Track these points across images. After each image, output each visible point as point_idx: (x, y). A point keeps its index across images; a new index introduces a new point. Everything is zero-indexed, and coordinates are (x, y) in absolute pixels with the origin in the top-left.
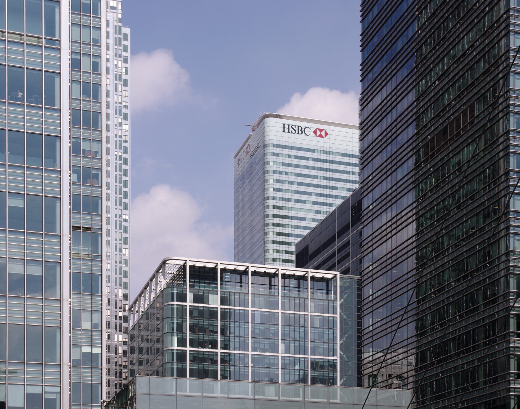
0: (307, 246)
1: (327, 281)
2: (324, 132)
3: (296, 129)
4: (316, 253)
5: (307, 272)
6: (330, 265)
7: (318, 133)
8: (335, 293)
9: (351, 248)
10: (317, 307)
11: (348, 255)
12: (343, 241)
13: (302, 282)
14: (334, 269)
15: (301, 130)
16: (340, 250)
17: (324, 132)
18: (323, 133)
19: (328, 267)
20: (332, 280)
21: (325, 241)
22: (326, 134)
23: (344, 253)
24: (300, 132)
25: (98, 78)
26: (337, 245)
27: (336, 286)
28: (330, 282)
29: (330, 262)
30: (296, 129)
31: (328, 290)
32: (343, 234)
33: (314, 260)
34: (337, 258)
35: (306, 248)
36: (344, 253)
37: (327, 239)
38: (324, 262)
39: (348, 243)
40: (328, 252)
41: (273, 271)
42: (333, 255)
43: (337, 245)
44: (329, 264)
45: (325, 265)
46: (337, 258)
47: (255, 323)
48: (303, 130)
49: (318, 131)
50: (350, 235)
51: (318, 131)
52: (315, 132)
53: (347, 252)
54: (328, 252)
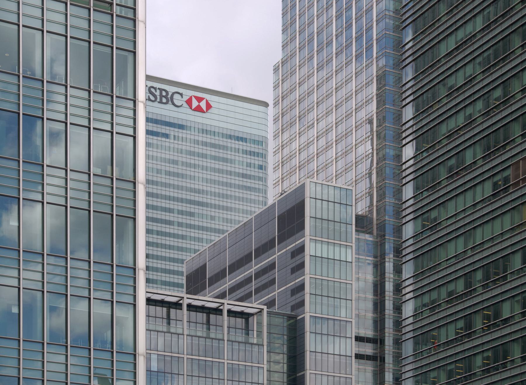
0: (205, 266)
1: (245, 316)
2: (204, 102)
3: (158, 93)
4: (220, 276)
5: (182, 298)
6: (242, 294)
7: (195, 103)
8: (260, 333)
9: (276, 274)
10: (195, 348)
11: (272, 282)
12: (265, 263)
13: (173, 311)
14: (249, 300)
15: (166, 97)
16: (258, 275)
17: (204, 102)
18: (203, 105)
19: (238, 297)
20: (255, 317)
21: (234, 260)
22: (209, 106)
23: (265, 279)
24: (164, 100)
25: (261, 115)
26: (254, 268)
27: (260, 324)
28: (250, 319)
29: (242, 289)
30: (158, 93)
31: (247, 330)
32: (263, 253)
33: (215, 285)
34: (253, 286)
35: (203, 268)
36: (265, 279)
37: (238, 258)
38: (232, 290)
39: (272, 266)
40: (240, 276)
41: (174, 300)
42: (248, 280)
43: (254, 268)
44: (241, 292)
45: (234, 294)
46: (253, 286)
47: (151, 371)
48: (169, 96)
49: (194, 100)
50: (276, 255)
51: (194, 100)
52: (189, 102)
53: (271, 278)
54: (240, 276)
